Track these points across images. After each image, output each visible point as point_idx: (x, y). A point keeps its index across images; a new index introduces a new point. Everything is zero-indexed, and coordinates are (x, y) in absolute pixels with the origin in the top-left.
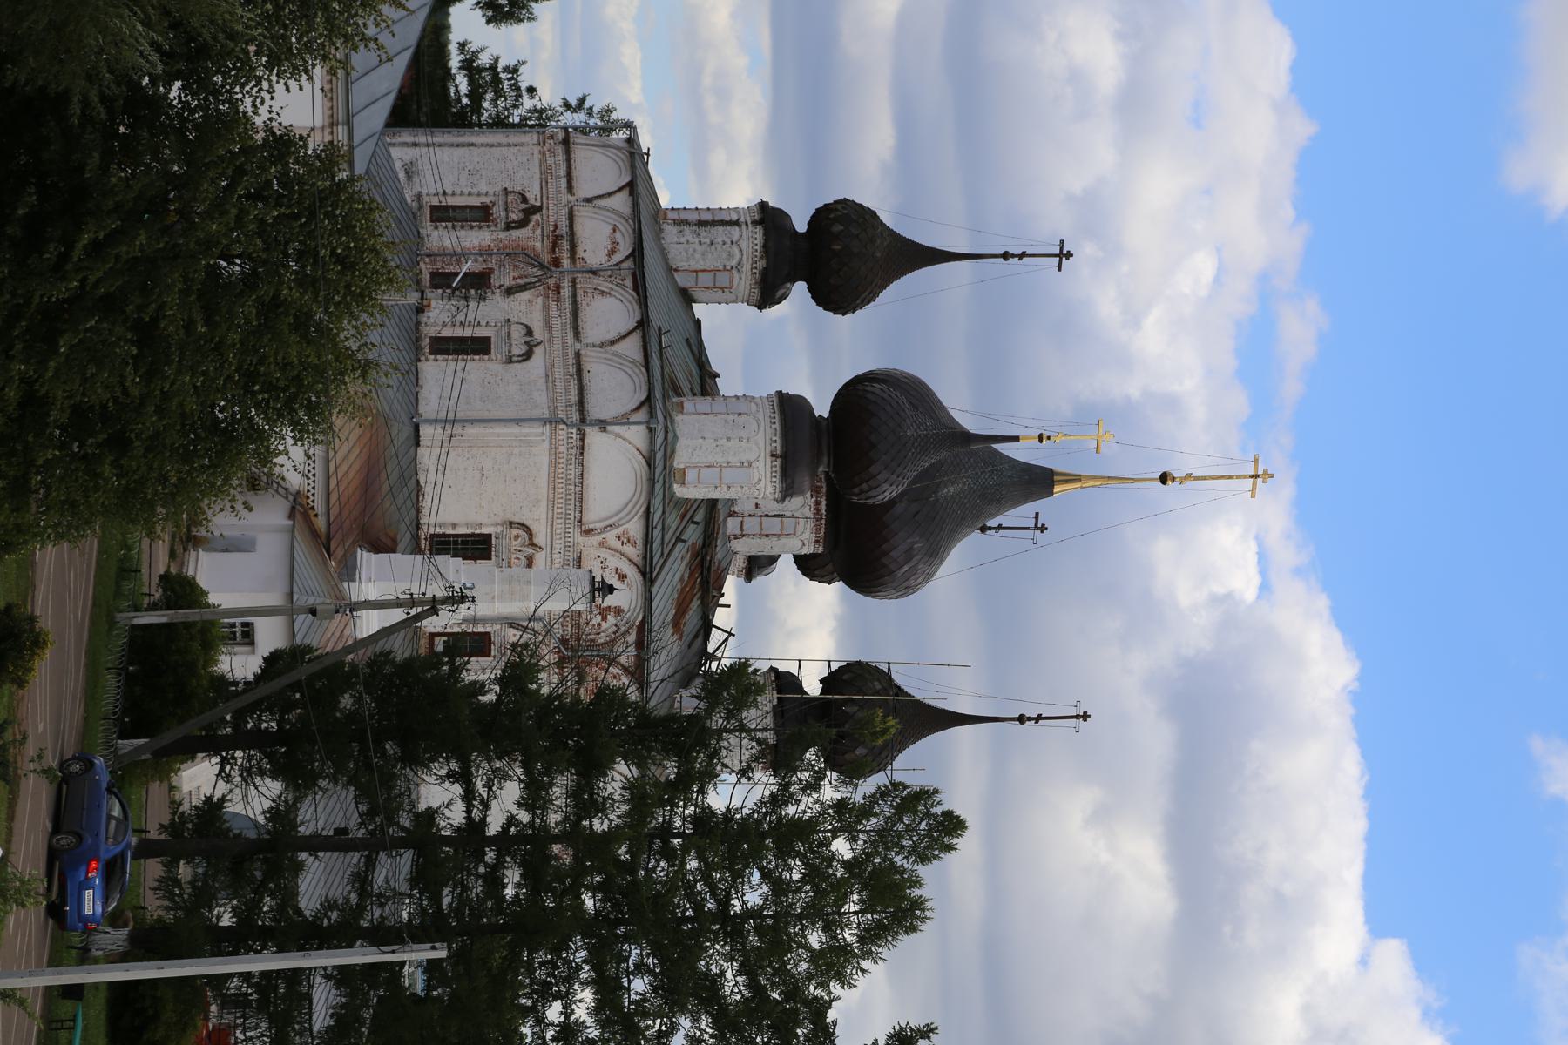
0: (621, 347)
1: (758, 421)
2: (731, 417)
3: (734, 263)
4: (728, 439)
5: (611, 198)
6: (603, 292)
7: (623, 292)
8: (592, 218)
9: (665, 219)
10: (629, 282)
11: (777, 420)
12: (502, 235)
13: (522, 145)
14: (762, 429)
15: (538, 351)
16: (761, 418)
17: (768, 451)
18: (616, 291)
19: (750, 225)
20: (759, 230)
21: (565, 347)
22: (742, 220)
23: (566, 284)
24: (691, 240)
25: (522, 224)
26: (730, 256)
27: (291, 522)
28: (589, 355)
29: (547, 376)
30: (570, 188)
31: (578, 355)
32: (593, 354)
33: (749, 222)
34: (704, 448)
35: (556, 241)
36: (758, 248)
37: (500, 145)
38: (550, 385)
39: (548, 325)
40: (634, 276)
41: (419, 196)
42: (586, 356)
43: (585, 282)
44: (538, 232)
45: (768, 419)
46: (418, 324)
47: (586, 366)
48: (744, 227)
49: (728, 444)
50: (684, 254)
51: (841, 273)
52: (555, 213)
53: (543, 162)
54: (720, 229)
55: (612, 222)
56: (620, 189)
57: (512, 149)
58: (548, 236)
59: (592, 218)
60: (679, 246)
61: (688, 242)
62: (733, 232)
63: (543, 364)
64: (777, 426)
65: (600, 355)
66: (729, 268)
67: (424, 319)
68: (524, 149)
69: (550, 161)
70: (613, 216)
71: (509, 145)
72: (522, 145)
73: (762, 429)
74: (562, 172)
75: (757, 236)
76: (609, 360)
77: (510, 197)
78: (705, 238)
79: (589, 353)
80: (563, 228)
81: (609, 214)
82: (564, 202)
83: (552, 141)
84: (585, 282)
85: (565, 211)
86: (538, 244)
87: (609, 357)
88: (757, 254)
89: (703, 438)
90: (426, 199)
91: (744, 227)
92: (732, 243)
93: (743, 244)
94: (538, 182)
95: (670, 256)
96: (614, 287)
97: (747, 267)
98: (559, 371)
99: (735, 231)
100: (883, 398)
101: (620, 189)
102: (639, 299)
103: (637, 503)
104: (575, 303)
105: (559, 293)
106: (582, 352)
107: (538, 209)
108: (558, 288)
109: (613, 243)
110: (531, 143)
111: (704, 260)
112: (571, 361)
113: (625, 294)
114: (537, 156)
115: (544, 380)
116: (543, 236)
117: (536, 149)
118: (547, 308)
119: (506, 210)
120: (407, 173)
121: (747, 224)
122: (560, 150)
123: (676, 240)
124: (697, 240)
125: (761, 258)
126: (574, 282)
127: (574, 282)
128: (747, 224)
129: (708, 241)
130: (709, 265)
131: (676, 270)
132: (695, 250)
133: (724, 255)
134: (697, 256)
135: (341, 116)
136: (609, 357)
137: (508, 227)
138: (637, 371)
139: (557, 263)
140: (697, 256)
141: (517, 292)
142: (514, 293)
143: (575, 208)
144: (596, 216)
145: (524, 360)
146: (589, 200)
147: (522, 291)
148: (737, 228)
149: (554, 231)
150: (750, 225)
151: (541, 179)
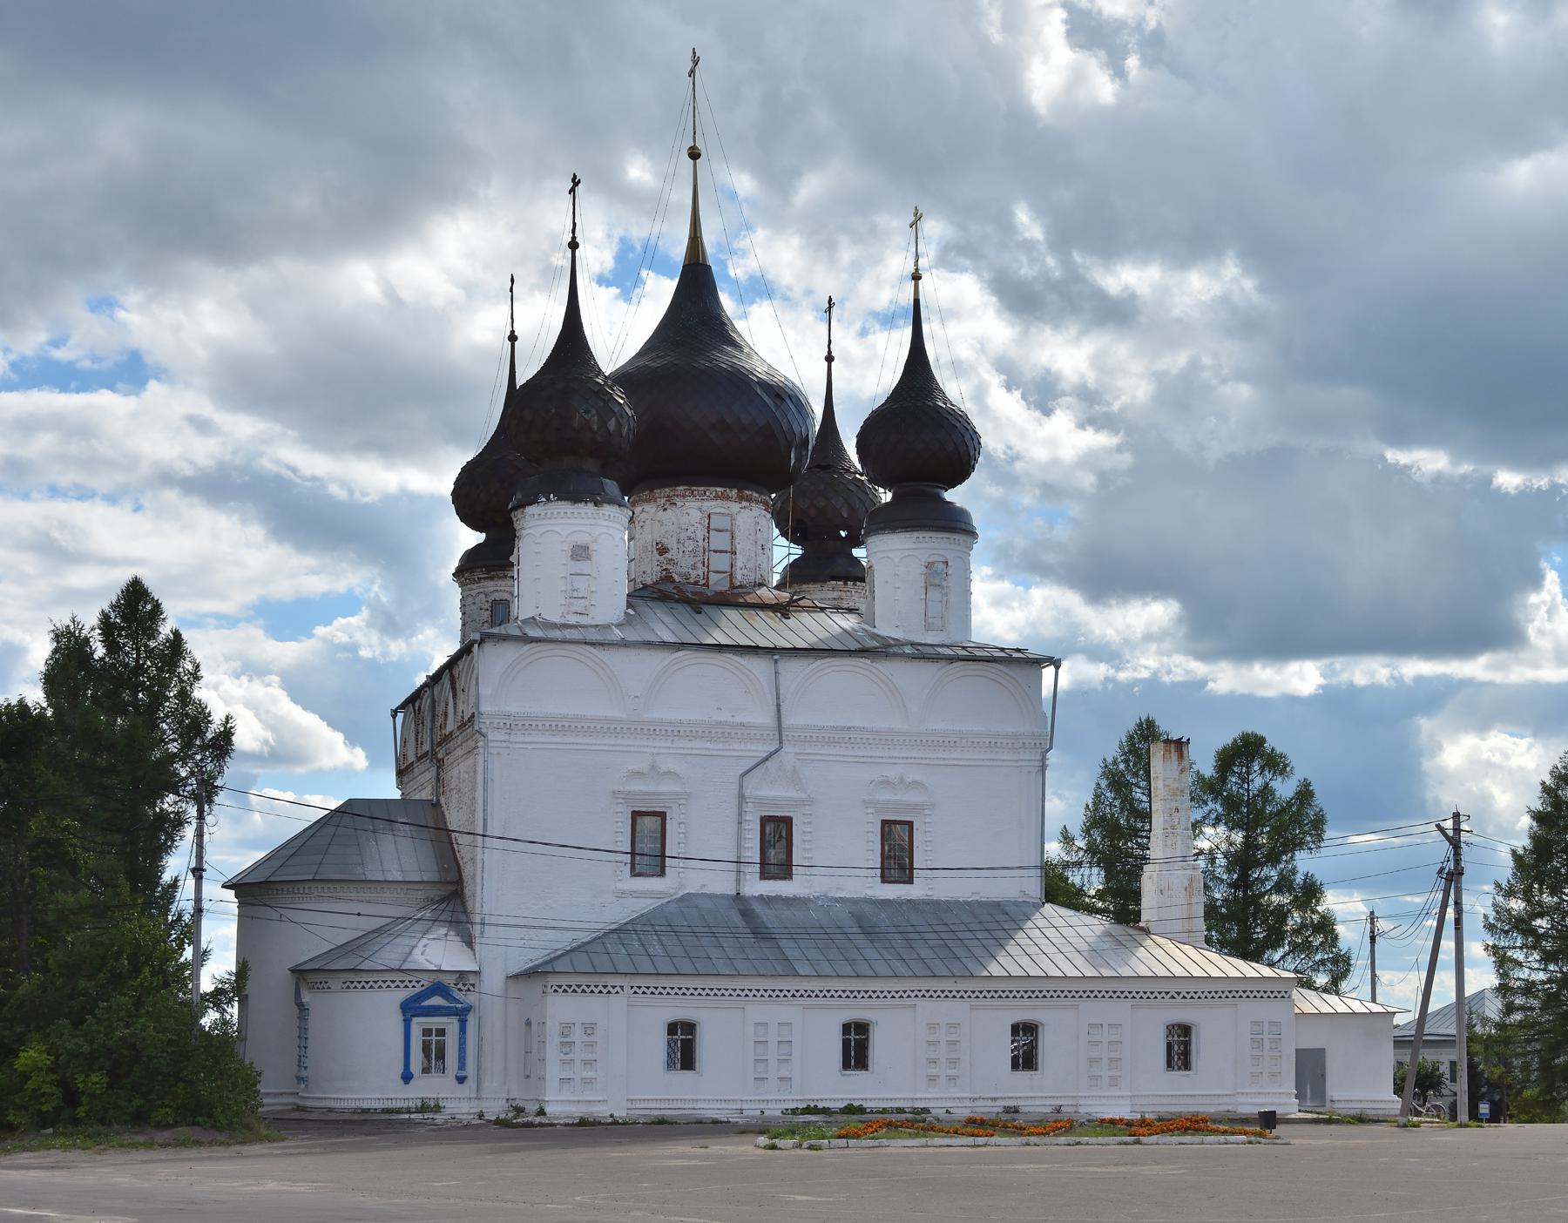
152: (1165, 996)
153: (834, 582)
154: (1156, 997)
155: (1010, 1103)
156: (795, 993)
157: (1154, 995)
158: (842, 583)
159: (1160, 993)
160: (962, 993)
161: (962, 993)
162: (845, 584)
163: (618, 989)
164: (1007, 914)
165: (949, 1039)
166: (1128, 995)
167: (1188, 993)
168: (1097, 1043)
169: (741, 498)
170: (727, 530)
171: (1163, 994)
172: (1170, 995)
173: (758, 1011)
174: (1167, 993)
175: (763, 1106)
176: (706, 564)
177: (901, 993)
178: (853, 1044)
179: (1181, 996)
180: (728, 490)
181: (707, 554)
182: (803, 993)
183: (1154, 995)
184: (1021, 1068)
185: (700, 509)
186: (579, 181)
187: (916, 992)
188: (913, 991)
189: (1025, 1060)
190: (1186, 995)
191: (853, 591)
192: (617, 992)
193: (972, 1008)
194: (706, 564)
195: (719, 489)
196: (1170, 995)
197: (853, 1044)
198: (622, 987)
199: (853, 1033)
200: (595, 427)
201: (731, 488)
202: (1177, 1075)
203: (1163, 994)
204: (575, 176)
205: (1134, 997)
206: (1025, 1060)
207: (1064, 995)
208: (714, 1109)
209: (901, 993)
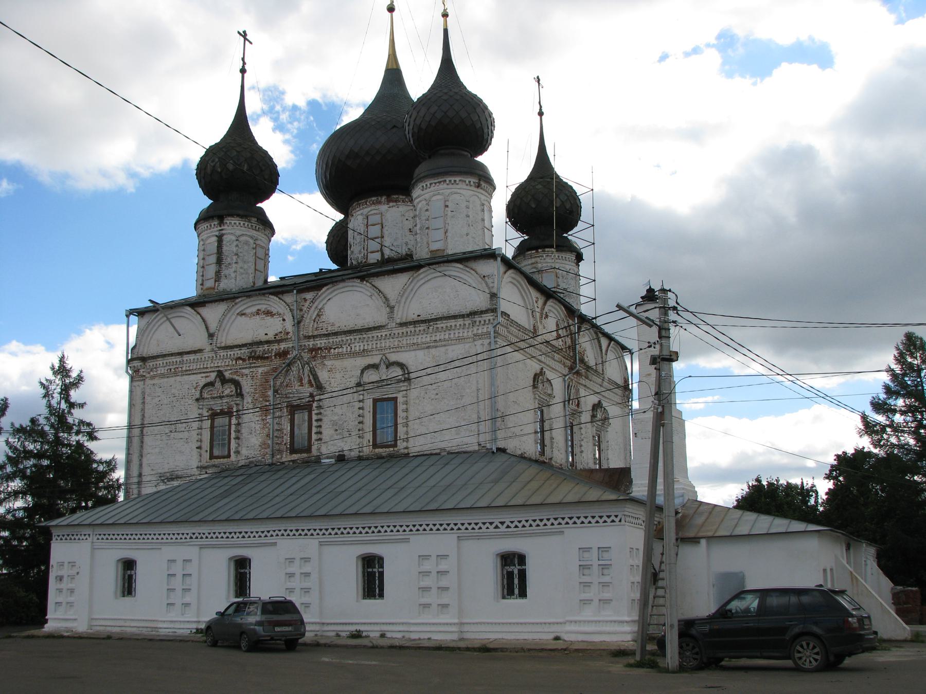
0: (392, 295)
1: (452, 193)
2: (449, 213)
3: (251, 241)
4: (468, 216)
5: (206, 319)
6: (318, 315)
7: (321, 298)
8: (227, 334)
9: (214, 288)
10: (309, 296)
11: (453, 179)
12: (248, 399)
13: (143, 393)
14: (459, 191)
15: (393, 358)
16: (449, 191)
17: (475, 189)
18: (319, 304)
19: (222, 228)
20: (228, 220)
21: (391, 336)
22: (217, 233)
23: (311, 343)
24: (233, 270)
25: (237, 384)
26: (247, 243)
27: (703, 542)
28: (400, 316)
29: (428, 347)
30: (200, 351)
31: (402, 325)
32: (400, 313)
33: (220, 228)
34: (474, 235)
35: (255, 357)
36: (242, 223)
37: (143, 410)
38: (438, 344)
39: (364, 353)
40: (300, 291)
41: (200, 468)
42: (401, 319)
43: (309, 327)
44: (246, 371)
45: (450, 186)
46: (360, 459)
47: (412, 317)
48: (223, 232)
49: (471, 216)
50: (243, 276)
51: (263, 168)
52: (224, 362)
53: (163, 376)
54: (225, 248)
55: (234, 317)
56: (198, 313)
57: (147, 401)
58: (251, 364)
59: (227, 334)
60: (238, 279)
61: (235, 272)
62: (228, 239)
63: (413, 353)
64: (458, 179)
65: (401, 308)
66: (255, 245)
67: (354, 454)
68: (148, 391)
69: (161, 371)
70: (229, 316)
71: (144, 403)
72: (143, 393)
73: (459, 191)
74: (178, 359)
75: (233, 222)
76: (407, 298)
77: (205, 395)
78: (232, 259)
79: (399, 316)
80: (245, 352)
81: (227, 319)
82: (212, 354)
83: (141, 371)
84: (309, 327)
85: (222, 353)
86: (260, 370)
87: (403, 300)
88: (246, 224)
89: (467, 235)
90: (204, 463)
91: (223, 232)
92: (237, 240)
93: (238, 233)
94: (186, 377)
95: (245, 287)
96: (315, 305)
97: (254, 233)
98: (426, 338)
99: (226, 238)
100: (409, 125)
101: (198, 313)
102: (332, 283)
103: (524, 290)
104: (336, 334)
105: (320, 349)
106: (398, 321)
107: (220, 374)
108: (315, 350)
109: (258, 314)
110: (142, 386)
111: (248, 262)
112: (404, 330)
113: (324, 295)
114: (156, 381)
115: (433, 351)
116: (250, 367)
117: (148, 382)
118: (340, 356)
119: (221, 397)
120: (172, 479)
121: (222, 230)
122: (151, 364)
123: (233, 280)
124: (234, 265)
125: (249, 221)
126: (309, 337)
127: (309, 337)
128: (222, 230)
129: (235, 258)
130: (252, 259)
131: (254, 284)
132: (241, 268)
133: (246, 247)
134: (246, 266)
135: (567, 399)
136: (403, 300)
137: (240, 395)
138: (422, 276)
139: (283, 354)
140: (246, 266)
141: (319, 381)
142: (321, 384)
143: (218, 345)
144: (226, 331)
145: (404, 365)
146: (211, 336)
147: (318, 378)
148: (225, 237)
149: (244, 360)
150: (222, 228)
151: (182, 375)
152: (489, 526)
153: (530, 252)
154: (480, 528)
155: (353, 628)
156: (192, 536)
157: (478, 526)
158: (534, 251)
159: (484, 524)
160: (312, 531)
161: (312, 531)
162: (537, 252)
163: (87, 536)
164: (201, 456)
165: (303, 571)
166: (454, 527)
167: (512, 522)
168: (291, 575)
169: (389, 201)
170: (378, 224)
171: (488, 525)
172: (494, 525)
173: (169, 552)
174: (491, 523)
175: (385, 628)
176: (366, 249)
177: (266, 533)
178: (377, 575)
179: (505, 525)
180: (379, 198)
181: (366, 242)
182: (198, 535)
183: (478, 526)
184: (377, 597)
185: (362, 214)
186: (244, 32)
187: (277, 532)
188: (274, 531)
189: (128, 587)
190: (510, 524)
191: (544, 255)
192: (86, 539)
193: (321, 544)
194: (366, 249)
195: (373, 199)
196: (494, 525)
197: (377, 575)
198: (89, 535)
199: (377, 566)
200: (219, 170)
201: (381, 196)
202: (515, 602)
203: (488, 525)
204: (239, 33)
205: (459, 529)
206: (128, 587)
207: (396, 529)
208: (183, 629)
209: (266, 533)
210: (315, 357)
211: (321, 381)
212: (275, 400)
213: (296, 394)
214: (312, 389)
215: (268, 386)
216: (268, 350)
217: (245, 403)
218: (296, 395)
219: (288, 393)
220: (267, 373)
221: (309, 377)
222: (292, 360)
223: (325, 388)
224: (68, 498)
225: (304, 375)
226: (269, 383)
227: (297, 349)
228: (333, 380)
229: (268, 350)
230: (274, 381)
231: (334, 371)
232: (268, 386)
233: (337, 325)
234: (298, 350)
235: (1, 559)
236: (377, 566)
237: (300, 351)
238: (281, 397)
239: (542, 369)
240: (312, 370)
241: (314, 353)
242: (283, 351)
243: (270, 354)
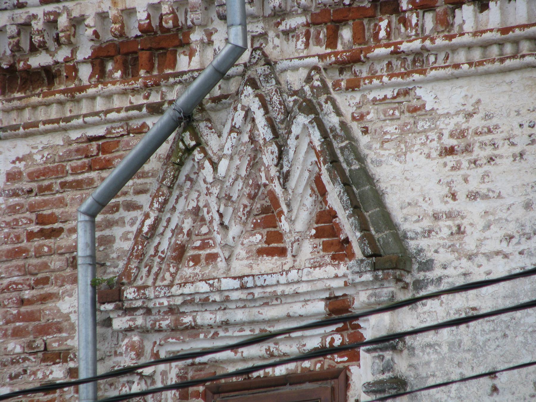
72: (44, 123)
210: (355, 60)
211: (398, 216)
212: (104, 347)
213: (244, 304)
214: (342, 269)
215: (56, 262)
216: (52, 23)
217: (182, 178)
218: (240, 315)
219: (189, 301)
220: (44, 173)
221: (322, 192)
222: (208, 86)
223: (427, 265)
224: (348, 52)
225: (285, 177)
226: (64, 241)
227: (235, 15)
228: (480, 205)
229: (52, 23)
230: (94, 226)
231: (478, 153)
232: (56, 262)
233: (122, 365)
234: (246, 18)
235: (420, 1)
236: (332, 12)
237: (257, 28)
238: (144, 331)
239: (278, 46)
240: (337, 145)
241: (346, 34)
242: (146, 30)
243: (62, 54)
